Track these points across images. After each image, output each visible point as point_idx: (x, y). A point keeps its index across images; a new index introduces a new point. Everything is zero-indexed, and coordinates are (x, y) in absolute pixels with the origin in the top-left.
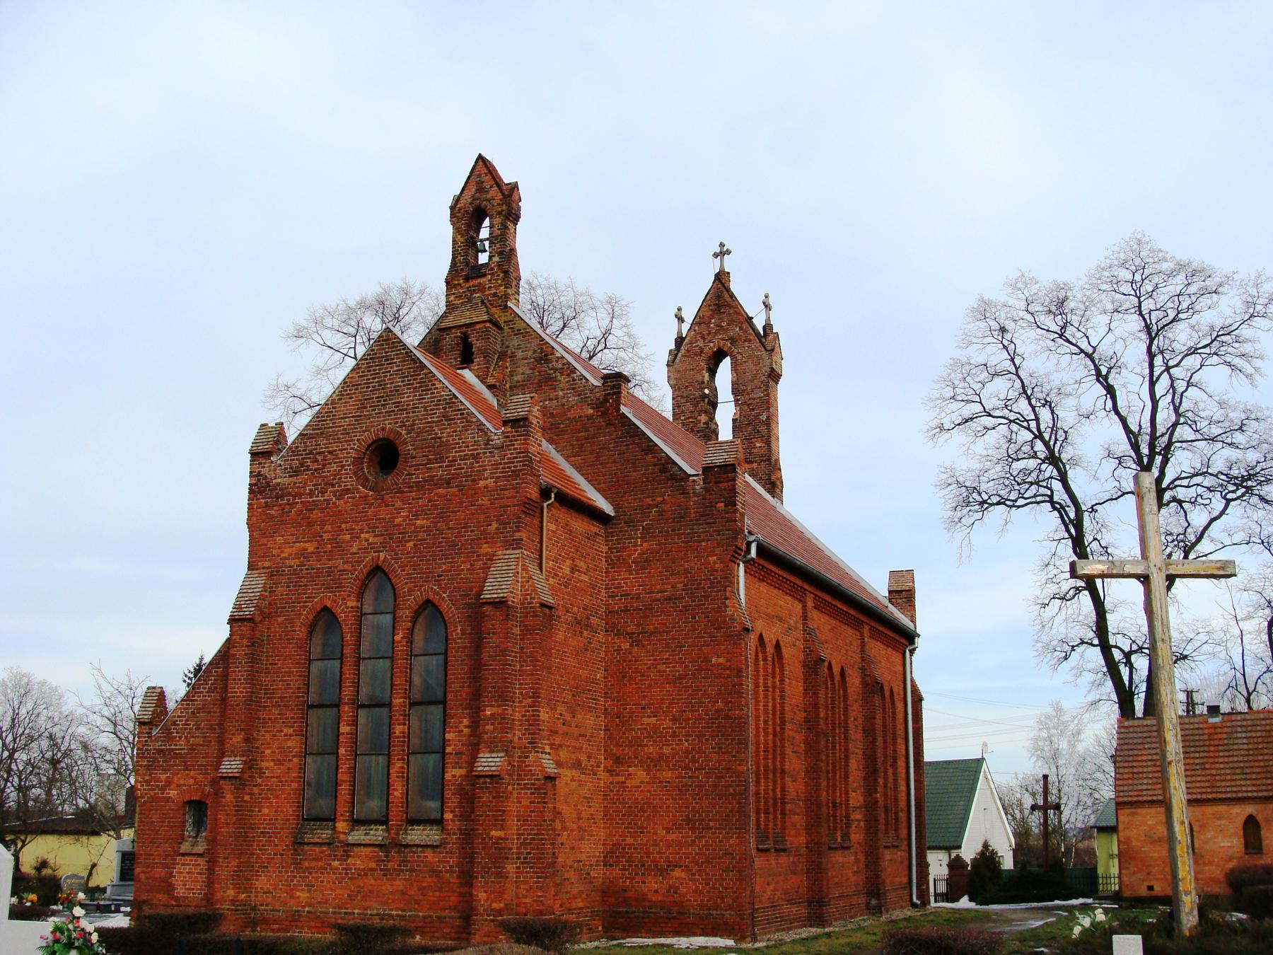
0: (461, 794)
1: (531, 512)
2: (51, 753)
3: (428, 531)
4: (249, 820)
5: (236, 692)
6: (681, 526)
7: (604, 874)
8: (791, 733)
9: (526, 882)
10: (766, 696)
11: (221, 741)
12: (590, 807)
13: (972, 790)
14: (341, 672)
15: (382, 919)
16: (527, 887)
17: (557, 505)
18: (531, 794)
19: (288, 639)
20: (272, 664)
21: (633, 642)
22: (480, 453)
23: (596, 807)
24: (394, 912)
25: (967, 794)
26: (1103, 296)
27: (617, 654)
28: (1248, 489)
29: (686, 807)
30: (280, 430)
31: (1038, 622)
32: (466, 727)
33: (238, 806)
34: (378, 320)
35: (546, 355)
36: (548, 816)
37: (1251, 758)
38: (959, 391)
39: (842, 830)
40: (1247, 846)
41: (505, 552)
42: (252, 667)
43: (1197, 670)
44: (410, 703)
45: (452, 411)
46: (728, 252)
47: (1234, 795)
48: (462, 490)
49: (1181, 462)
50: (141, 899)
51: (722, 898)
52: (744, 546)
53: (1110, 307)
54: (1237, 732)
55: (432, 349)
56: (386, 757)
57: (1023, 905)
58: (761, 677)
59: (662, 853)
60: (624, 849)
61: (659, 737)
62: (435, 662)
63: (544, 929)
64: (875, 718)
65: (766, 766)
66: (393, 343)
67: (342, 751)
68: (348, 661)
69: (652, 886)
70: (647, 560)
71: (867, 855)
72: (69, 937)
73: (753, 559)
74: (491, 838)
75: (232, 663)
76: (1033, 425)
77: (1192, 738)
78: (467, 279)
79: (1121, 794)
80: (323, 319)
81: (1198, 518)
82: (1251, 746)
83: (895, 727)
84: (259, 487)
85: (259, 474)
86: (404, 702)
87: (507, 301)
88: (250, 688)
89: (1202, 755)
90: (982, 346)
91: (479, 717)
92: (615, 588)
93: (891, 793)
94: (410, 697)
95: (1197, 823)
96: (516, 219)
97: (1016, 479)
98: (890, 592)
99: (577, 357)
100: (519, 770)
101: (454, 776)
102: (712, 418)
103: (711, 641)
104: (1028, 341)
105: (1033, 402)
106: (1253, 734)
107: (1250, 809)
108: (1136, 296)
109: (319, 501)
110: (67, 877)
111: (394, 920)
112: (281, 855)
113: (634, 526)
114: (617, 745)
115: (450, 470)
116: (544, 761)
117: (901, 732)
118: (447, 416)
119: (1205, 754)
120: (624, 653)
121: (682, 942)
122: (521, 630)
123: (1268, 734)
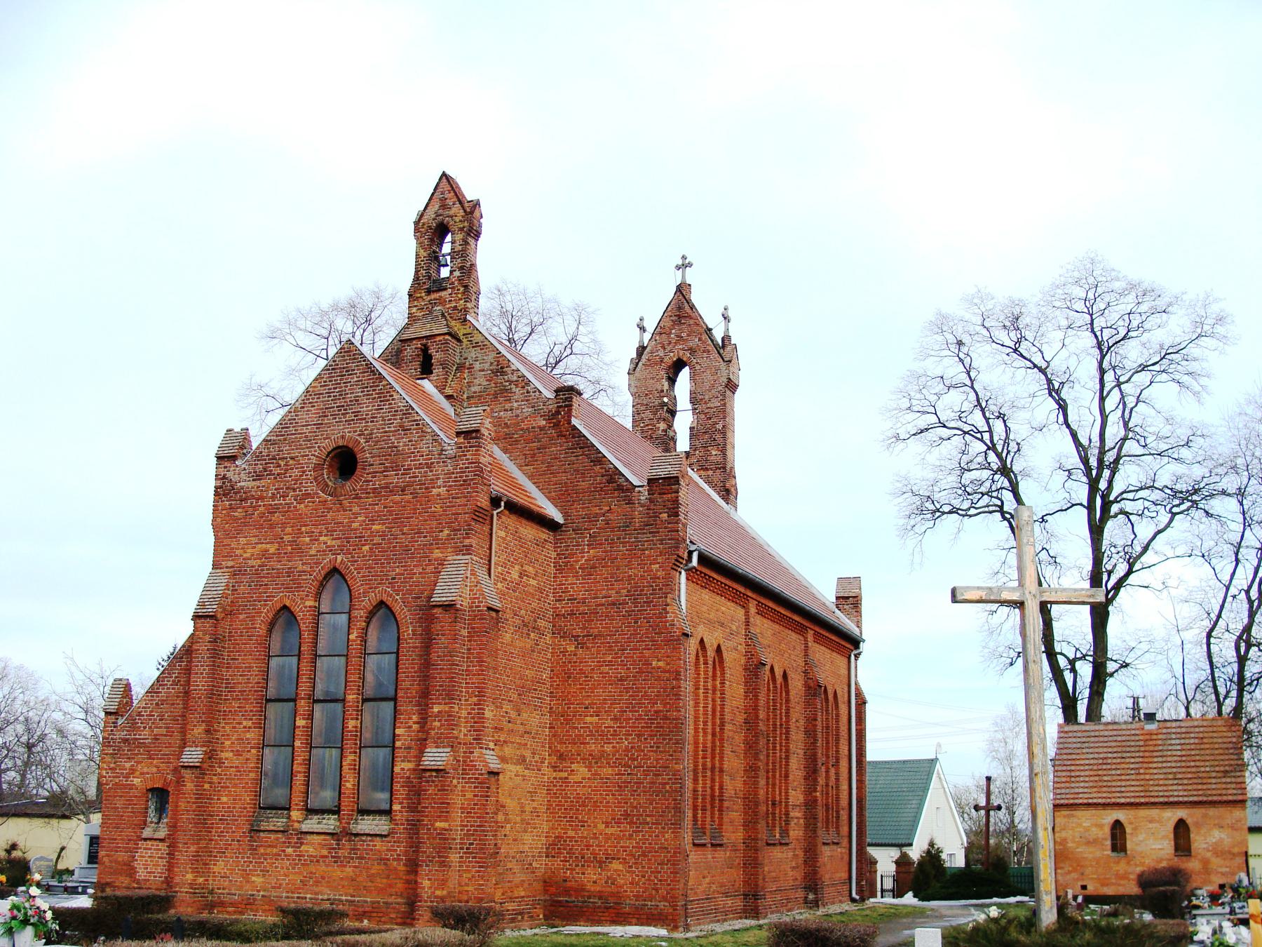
0: (408, 787)
1: (481, 520)
2: (26, 737)
3: (383, 536)
4: (208, 807)
5: (198, 686)
6: (626, 534)
7: (546, 864)
8: (731, 734)
9: (469, 871)
10: (706, 698)
11: (183, 732)
12: (533, 801)
13: (925, 789)
14: (298, 668)
15: (332, 904)
16: (470, 876)
17: (507, 512)
18: (475, 787)
19: (248, 636)
20: (232, 659)
21: (578, 644)
22: (433, 463)
23: (538, 801)
24: (344, 898)
25: (921, 793)
26: (1058, 312)
27: (563, 656)
28: (1194, 502)
29: (624, 803)
30: (245, 435)
31: (987, 627)
32: (415, 723)
33: (197, 794)
34: (350, 323)
35: (502, 368)
36: (491, 809)
37: (1183, 764)
38: (914, 402)
39: (781, 827)
40: (1177, 848)
41: (455, 557)
42: (214, 661)
43: (1139, 677)
44: (363, 699)
45: (408, 422)
46: (690, 265)
47: (1166, 800)
48: (417, 497)
49: (1128, 476)
50: (103, 881)
51: (657, 890)
52: (686, 556)
53: (1064, 323)
54: (1171, 739)
55: (394, 360)
56: (340, 750)
57: (963, 902)
58: (702, 680)
59: (601, 846)
60: (565, 841)
61: (600, 735)
62: (388, 660)
63: (468, 915)
64: (816, 720)
65: (704, 765)
66: (354, 355)
67: (297, 743)
68: (305, 658)
69: (591, 878)
70: (594, 567)
71: (806, 852)
72: (26, 914)
73: (694, 568)
74: (435, 829)
75: (195, 658)
76: (986, 436)
77: (1128, 744)
78: (429, 292)
79: (1058, 797)
80: (296, 320)
81: (1145, 530)
82: (1184, 753)
83: (838, 729)
84: (224, 490)
85: (224, 477)
86: (357, 698)
87: (466, 315)
88: (212, 681)
89: (1137, 760)
90: (939, 359)
91: (427, 714)
92: (562, 592)
93: (832, 792)
94: (363, 693)
95: (1130, 826)
96: (477, 235)
97: (967, 489)
98: (838, 598)
99: (532, 367)
100: (466, 766)
101: (403, 769)
102: (670, 427)
103: (652, 645)
104: (986, 358)
105: (987, 415)
106: (1187, 741)
107: (1181, 813)
108: (1089, 313)
109: (281, 504)
110: (36, 859)
111: (343, 905)
112: (238, 841)
113: (581, 534)
114: (561, 743)
115: (405, 478)
116: (487, 757)
117: (843, 732)
118: (403, 426)
119: (1141, 760)
120: (569, 655)
121: (617, 931)
122: (468, 632)
123: (1200, 741)
